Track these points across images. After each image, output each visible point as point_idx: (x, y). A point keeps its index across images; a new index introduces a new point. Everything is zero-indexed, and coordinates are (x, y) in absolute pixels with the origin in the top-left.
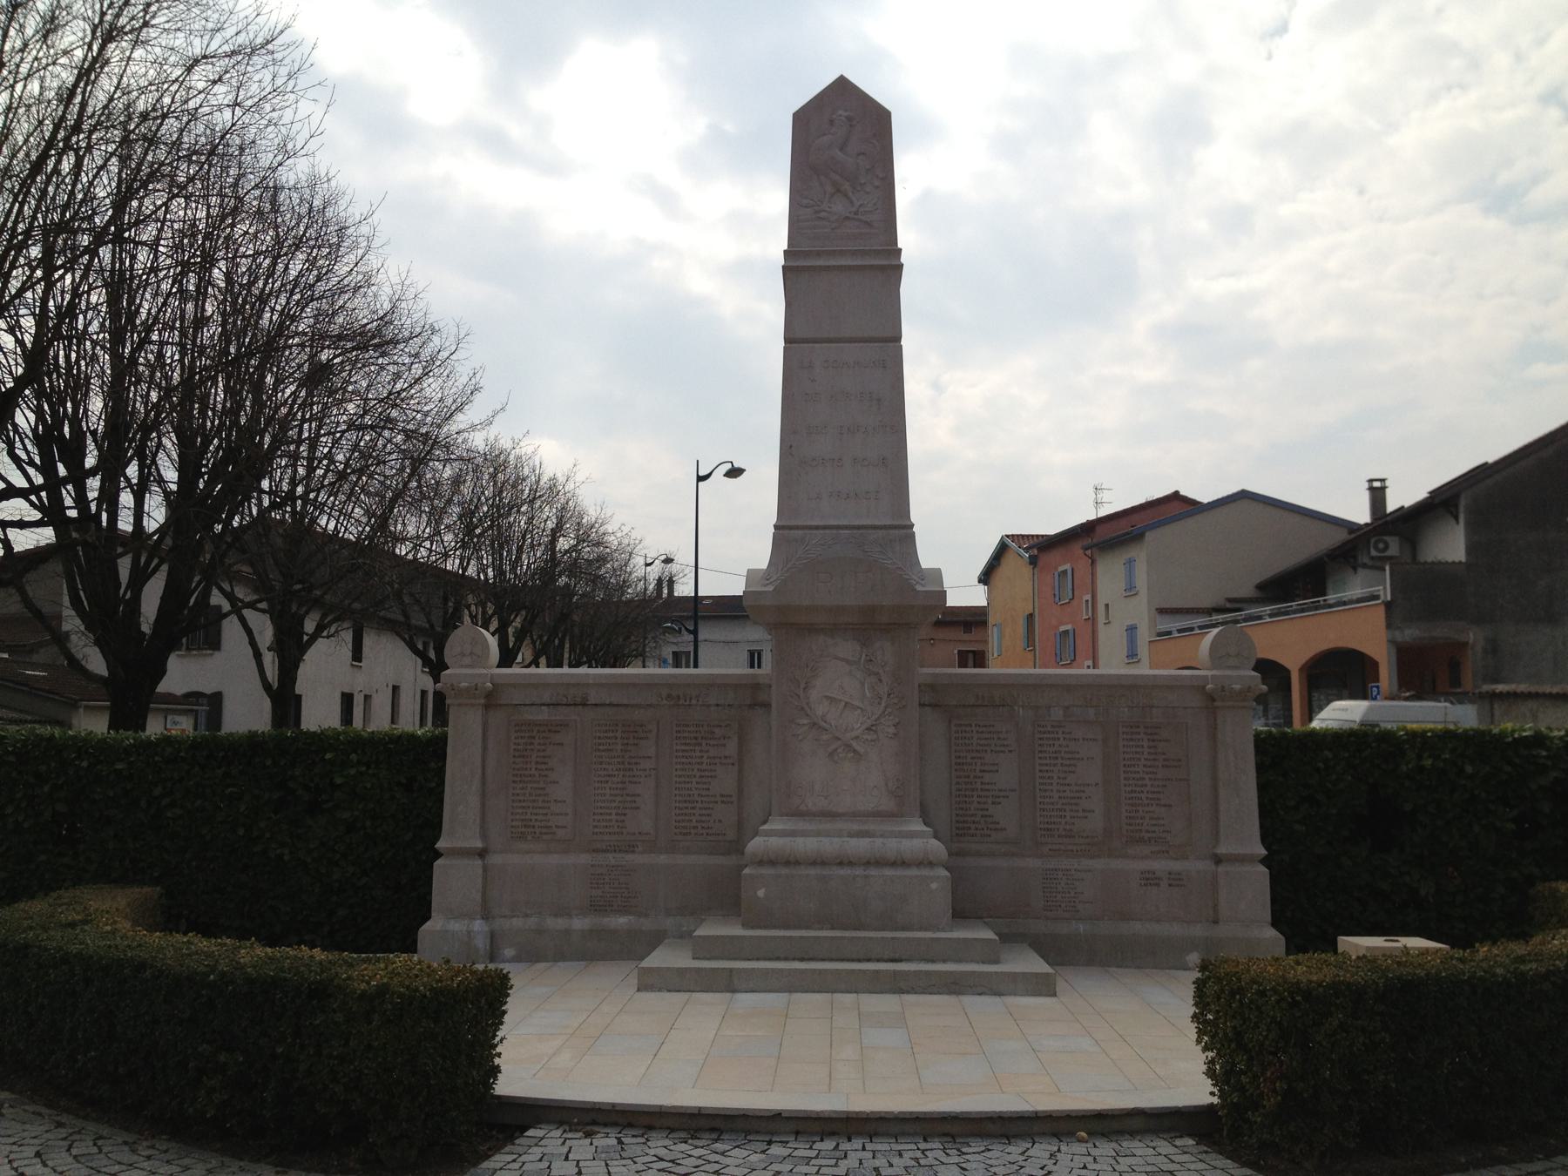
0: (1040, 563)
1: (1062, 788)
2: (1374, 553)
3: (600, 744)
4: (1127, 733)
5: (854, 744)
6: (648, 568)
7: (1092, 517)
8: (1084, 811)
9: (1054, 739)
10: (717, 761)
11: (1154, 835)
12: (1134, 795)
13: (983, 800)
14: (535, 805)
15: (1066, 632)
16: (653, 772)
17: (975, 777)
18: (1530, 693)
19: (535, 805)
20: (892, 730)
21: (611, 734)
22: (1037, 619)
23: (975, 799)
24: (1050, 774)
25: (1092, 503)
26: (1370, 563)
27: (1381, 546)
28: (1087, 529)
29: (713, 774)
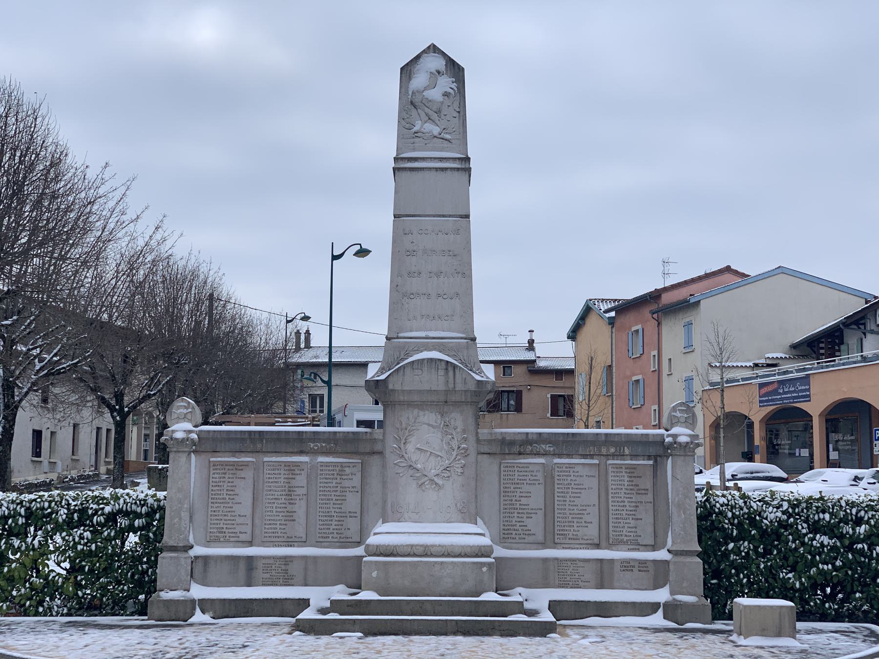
0: (618, 323)
1: (572, 508)
3: (269, 478)
4: (614, 472)
5: (436, 479)
7: (660, 286)
8: (585, 522)
10: (347, 489)
11: (630, 538)
12: (618, 512)
13: (520, 515)
14: (226, 518)
15: (637, 381)
16: (304, 497)
17: (516, 500)
19: (226, 518)
20: (460, 470)
21: (277, 472)
22: (614, 368)
23: (516, 515)
24: (322, 502)
25: (661, 274)
28: (655, 296)
29: (344, 498)
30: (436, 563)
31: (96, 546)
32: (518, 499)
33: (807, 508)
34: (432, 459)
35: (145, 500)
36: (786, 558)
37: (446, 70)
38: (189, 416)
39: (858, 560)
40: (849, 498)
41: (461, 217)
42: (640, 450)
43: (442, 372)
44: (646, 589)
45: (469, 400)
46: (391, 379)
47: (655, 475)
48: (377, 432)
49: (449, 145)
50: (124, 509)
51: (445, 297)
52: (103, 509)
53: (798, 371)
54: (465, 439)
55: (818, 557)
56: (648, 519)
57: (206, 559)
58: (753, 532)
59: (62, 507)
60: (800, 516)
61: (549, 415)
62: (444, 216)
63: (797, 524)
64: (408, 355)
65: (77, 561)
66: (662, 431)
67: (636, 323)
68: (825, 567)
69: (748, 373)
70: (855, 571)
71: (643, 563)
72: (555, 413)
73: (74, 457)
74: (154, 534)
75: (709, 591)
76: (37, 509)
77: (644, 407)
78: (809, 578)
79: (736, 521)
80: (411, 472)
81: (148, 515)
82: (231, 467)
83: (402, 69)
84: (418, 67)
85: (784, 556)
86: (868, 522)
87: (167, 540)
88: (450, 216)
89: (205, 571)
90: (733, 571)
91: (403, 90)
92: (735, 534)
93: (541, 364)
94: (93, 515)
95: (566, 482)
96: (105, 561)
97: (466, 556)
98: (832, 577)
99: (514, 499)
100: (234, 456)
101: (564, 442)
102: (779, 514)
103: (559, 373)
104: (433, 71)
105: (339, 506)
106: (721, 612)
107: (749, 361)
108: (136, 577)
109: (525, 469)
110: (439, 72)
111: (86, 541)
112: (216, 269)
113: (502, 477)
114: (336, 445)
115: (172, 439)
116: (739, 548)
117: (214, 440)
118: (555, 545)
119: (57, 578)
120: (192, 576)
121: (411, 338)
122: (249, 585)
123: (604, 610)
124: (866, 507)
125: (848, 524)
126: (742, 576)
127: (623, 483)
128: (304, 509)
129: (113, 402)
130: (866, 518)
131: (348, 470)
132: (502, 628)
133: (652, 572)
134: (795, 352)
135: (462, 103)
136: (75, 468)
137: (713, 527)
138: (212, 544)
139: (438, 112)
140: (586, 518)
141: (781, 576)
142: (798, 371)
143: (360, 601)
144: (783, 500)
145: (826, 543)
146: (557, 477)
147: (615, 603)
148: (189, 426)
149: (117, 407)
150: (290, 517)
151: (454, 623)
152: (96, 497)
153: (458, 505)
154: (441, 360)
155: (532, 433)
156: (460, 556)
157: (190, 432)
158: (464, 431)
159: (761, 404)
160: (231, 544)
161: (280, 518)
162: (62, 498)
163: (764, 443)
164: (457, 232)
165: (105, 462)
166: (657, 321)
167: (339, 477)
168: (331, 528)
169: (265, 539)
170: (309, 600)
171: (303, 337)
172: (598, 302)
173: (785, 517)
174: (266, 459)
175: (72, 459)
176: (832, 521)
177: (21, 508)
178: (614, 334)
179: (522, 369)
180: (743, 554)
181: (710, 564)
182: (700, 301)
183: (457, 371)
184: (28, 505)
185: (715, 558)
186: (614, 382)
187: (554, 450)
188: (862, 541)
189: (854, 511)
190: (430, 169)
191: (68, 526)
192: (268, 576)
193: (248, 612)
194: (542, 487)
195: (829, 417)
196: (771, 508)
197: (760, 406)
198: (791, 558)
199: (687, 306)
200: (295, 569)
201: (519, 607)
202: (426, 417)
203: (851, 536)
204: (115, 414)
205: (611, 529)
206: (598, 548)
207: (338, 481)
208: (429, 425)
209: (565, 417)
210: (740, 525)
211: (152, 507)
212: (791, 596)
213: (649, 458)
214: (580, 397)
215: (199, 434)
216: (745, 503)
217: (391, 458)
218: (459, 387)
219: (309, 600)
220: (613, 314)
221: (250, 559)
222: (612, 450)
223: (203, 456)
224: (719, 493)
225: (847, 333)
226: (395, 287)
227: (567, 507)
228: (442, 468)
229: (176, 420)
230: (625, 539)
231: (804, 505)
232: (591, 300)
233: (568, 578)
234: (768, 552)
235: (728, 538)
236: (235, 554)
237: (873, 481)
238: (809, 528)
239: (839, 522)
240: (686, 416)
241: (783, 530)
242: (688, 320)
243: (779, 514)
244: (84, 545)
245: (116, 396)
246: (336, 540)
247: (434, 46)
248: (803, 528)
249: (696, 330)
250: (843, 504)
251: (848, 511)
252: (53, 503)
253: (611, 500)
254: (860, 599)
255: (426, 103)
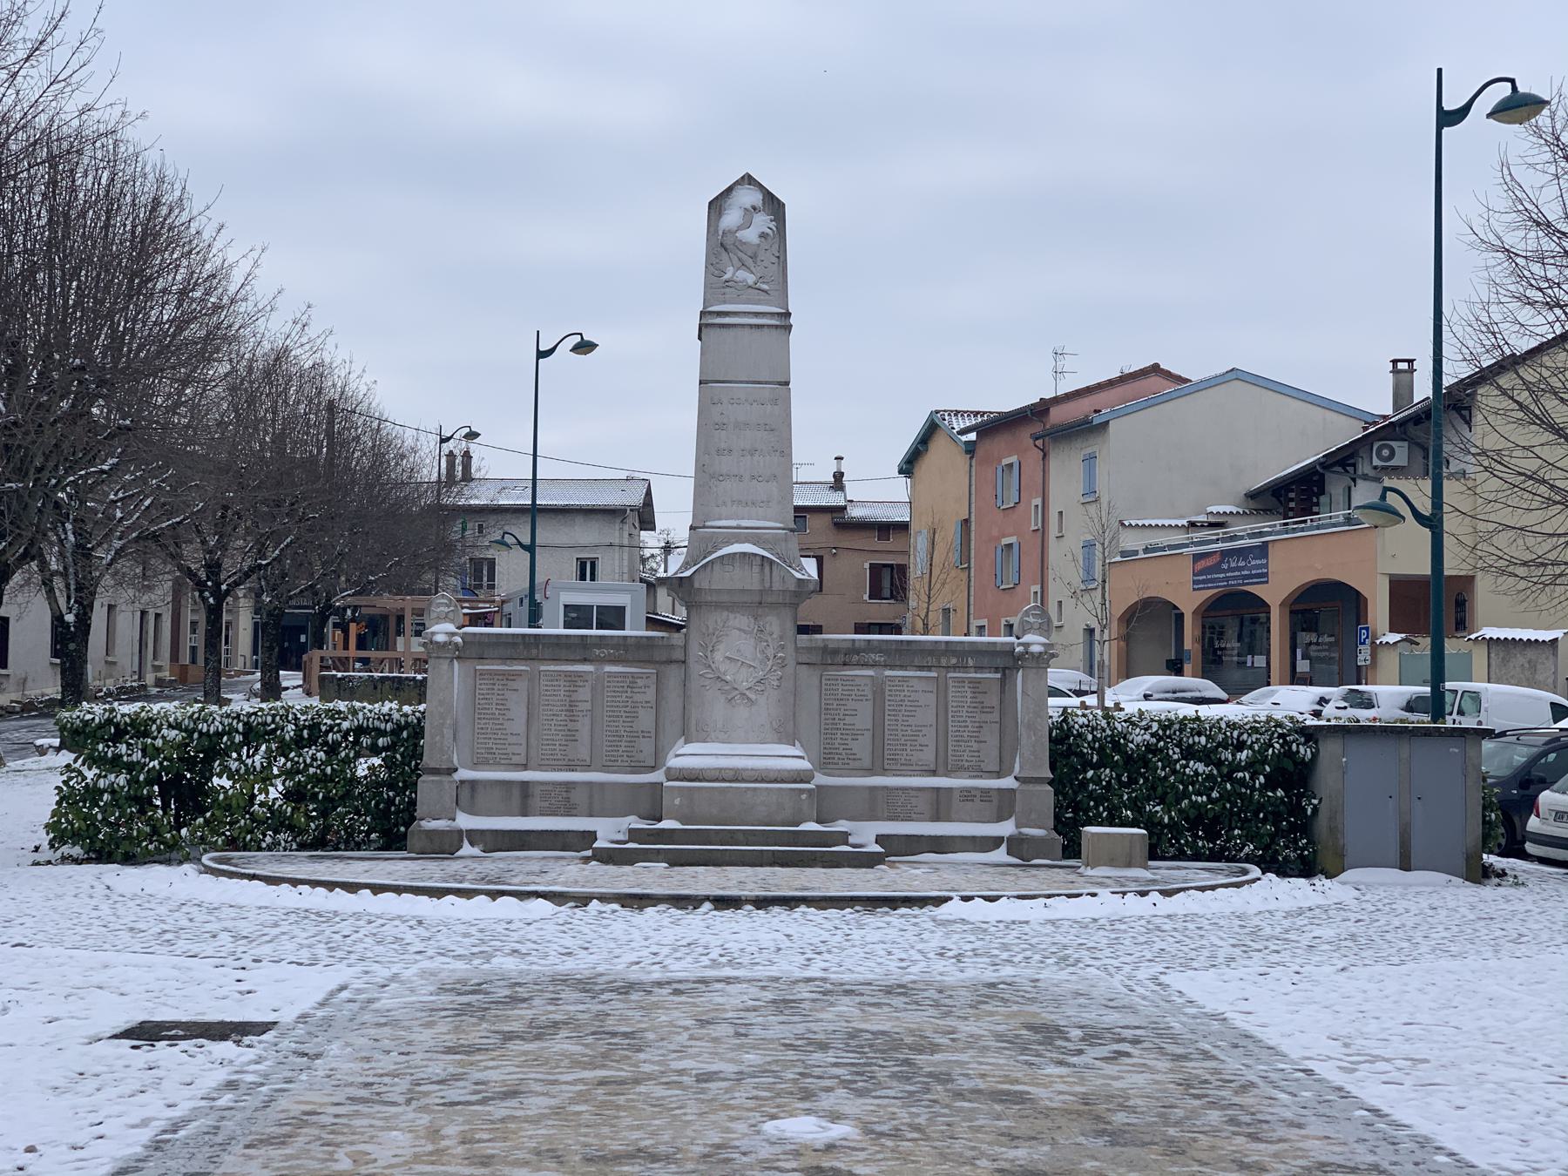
0: (980, 452)
2: (1376, 462)
5: (747, 693)
6: (444, 445)
7: (1049, 394)
9: (900, 691)
10: (640, 705)
13: (844, 737)
15: (1010, 546)
18: (1536, 641)
22: (973, 524)
26: (1371, 473)
27: (1386, 453)
28: (1040, 410)
30: (748, 789)
31: (332, 769)
32: (842, 717)
33: (1181, 730)
34: (744, 670)
35: (390, 715)
36: (1154, 788)
37: (764, 204)
38: (451, 615)
39: (1238, 791)
40: (1231, 718)
41: (780, 383)
42: (986, 661)
43: (756, 569)
44: (989, 822)
45: (787, 601)
46: (696, 577)
47: (1002, 692)
48: (677, 638)
49: (767, 297)
50: (365, 725)
51: (760, 479)
52: (340, 724)
53: (1252, 536)
54: (783, 647)
55: (1190, 788)
56: (993, 741)
57: (473, 784)
58: (1116, 758)
59: (289, 722)
60: (1172, 740)
61: (866, 597)
62: (759, 383)
63: (1168, 749)
64: (716, 548)
65: (309, 787)
66: (1012, 639)
67: (1012, 452)
68: (1199, 799)
69: (1179, 538)
70: (1234, 804)
71: (986, 792)
72: (875, 593)
73: (110, 659)
74: (402, 755)
75: (1060, 825)
76: (258, 724)
77: (1018, 588)
78: (1181, 811)
79: (1097, 745)
80: (719, 685)
81: (393, 732)
82: (500, 678)
83: (710, 203)
84: (729, 201)
85: (1152, 785)
86: (1251, 747)
87: (428, 760)
88: (766, 383)
89: (472, 797)
90: (1092, 803)
91: (712, 229)
92: (1095, 760)
93: (855, 513)
94: (327, 732)
95: (898, 698)
96: (343, 787)
97: (783, 781)
98: (1207, 810)
99: (837, 717)
100: (505, 664)
101: (896, 650)
102: (1147, 737)
103: (886, 529)
104: (749, 207)
105: (630, 724)
106: (1072, 850)
107: (1182, 517)
108: (382, 806)
109: (851, 683)
110: (754, 208)
111: (319, 763)
112: (359, 372)
113: (823, 692)
114: (626, 651)
115: (431, 642)
116: (1100, 777)
117: (480, 643)
118: (884, 772)
119: (285, 807)
120: (457, 803)
121: (720, 528)
122: (525, 814)
123: (940, 845)
124: (1250, 729)
125: (1227, 750)
126: (1101, 809)
127: (965, 699)
128: (587, 728)
129: (203, 575)
130: (1249, 743)
131: (640, 682)
132: (824, 859)
133: (995, 802)
134: (1253, 504)
135: (782, 249)
136: (111, 676)
137: (1070, 752)
138: (480, 767)
139: (754, 257)
140: (922, 740)
141: (1148, 809)
142: (1252, 536)
143: (663, 830)
144: (1152, 720)
145: (1200, 771)
146: (887, 693)
147: (952, 837)
148: (451, 627)
149: (209, 583)
150: (571, 736)
151: (771, 854)
152: (330, 710)
153: (774, 723)
154: (756, 555)
155: (860, 640)
156: (775, 781)
157: (453, 634)
158: (781, 638)
159: (1196, 587)
160: (502, 767)
161: (560, 737)
162: (288, 711)
163: (1198, 647)
164: (775, 402)
165: (153, 666)
166: (1042, 450)
167: (629, 690)
168: (621, 749)
169: (543, 762)
170: (595, 832)
171: (458, 460)
172: (949, 415)
173: (1154, 740)
174: (542, 668)
175: (106, 662)
176: (1209, 745)
177: (238, 723)
178: (973, 469)
179: (822, 522)
180: (1104, 783)
181: (1065, 795)
182: (1107, 422)
183: (774, 567)
184: (246, 720)
185: (1072, 788)
186: (973, 547)
187: (885, 661)
188: (1243, 769)
189: (1236, 734)
190: (743, 326)
191: (296, 744)
192: (546, 804)
193: (523, 845)
194: (871, 702)
195: (1293, 608)
196: (1138, 730)
197: (1194, 589)
198: (1160, 789)
199: (1088, 429)
200: (578, 797)
201: (843, 837)
202: (737, 620)
203: (1230, 763)
204: (207, 594)
205: (950, 753)
206: (934, 776)
207: (629, 694)
208: (740, 630)
209: (892, 601)
210: (1102, 749)
211: (398, 724)
212: (1158, 832)
213: (997, 670)
214: (916, 570)
215: (464, 636)
216: (1108, 723)
217: (696, 669)
218: (777, 586)
219: (595, 832)
220: (972, 436)
221: (525, 785)
222: (954, 661)
223: (468, 663)
224: (1079, 712)
225: (1329, 477)
226: (701, 467)
227: (900, 728)
228: (755, 680)
229: (435, 621)
230: (966, 764)
231: (1177, 726)
232: (937, 412)
233: (899, 810)
234: (1132, 781)
235: (1087, 764)
236: (507, 779)
237: (1343, 704)
238: (1181, 753)
239: (1217, 747)
240: (1040, 621)
241: (1150, 756)
242: (1089, 450)
243: (1147, 737)
244: (317, 768)
245: (208, 566)
246: (626, 764)
247: (749, 177)
248: (1174, 753)
249: (1101, 468)
250: (1223, 726)
251: (1228, 734)
252: (278, 718)
253: (950, 719)
254: (1240, 837)
255: (740, 245)
